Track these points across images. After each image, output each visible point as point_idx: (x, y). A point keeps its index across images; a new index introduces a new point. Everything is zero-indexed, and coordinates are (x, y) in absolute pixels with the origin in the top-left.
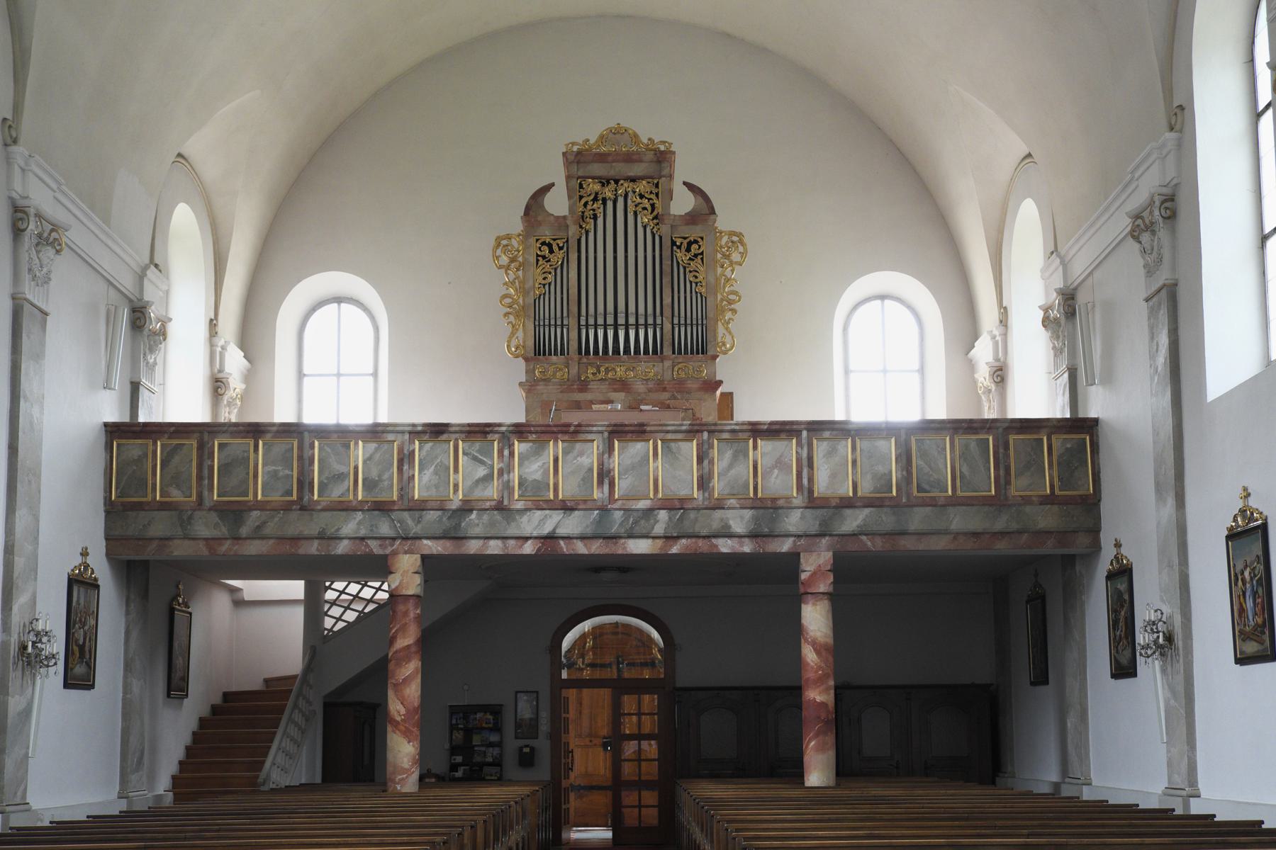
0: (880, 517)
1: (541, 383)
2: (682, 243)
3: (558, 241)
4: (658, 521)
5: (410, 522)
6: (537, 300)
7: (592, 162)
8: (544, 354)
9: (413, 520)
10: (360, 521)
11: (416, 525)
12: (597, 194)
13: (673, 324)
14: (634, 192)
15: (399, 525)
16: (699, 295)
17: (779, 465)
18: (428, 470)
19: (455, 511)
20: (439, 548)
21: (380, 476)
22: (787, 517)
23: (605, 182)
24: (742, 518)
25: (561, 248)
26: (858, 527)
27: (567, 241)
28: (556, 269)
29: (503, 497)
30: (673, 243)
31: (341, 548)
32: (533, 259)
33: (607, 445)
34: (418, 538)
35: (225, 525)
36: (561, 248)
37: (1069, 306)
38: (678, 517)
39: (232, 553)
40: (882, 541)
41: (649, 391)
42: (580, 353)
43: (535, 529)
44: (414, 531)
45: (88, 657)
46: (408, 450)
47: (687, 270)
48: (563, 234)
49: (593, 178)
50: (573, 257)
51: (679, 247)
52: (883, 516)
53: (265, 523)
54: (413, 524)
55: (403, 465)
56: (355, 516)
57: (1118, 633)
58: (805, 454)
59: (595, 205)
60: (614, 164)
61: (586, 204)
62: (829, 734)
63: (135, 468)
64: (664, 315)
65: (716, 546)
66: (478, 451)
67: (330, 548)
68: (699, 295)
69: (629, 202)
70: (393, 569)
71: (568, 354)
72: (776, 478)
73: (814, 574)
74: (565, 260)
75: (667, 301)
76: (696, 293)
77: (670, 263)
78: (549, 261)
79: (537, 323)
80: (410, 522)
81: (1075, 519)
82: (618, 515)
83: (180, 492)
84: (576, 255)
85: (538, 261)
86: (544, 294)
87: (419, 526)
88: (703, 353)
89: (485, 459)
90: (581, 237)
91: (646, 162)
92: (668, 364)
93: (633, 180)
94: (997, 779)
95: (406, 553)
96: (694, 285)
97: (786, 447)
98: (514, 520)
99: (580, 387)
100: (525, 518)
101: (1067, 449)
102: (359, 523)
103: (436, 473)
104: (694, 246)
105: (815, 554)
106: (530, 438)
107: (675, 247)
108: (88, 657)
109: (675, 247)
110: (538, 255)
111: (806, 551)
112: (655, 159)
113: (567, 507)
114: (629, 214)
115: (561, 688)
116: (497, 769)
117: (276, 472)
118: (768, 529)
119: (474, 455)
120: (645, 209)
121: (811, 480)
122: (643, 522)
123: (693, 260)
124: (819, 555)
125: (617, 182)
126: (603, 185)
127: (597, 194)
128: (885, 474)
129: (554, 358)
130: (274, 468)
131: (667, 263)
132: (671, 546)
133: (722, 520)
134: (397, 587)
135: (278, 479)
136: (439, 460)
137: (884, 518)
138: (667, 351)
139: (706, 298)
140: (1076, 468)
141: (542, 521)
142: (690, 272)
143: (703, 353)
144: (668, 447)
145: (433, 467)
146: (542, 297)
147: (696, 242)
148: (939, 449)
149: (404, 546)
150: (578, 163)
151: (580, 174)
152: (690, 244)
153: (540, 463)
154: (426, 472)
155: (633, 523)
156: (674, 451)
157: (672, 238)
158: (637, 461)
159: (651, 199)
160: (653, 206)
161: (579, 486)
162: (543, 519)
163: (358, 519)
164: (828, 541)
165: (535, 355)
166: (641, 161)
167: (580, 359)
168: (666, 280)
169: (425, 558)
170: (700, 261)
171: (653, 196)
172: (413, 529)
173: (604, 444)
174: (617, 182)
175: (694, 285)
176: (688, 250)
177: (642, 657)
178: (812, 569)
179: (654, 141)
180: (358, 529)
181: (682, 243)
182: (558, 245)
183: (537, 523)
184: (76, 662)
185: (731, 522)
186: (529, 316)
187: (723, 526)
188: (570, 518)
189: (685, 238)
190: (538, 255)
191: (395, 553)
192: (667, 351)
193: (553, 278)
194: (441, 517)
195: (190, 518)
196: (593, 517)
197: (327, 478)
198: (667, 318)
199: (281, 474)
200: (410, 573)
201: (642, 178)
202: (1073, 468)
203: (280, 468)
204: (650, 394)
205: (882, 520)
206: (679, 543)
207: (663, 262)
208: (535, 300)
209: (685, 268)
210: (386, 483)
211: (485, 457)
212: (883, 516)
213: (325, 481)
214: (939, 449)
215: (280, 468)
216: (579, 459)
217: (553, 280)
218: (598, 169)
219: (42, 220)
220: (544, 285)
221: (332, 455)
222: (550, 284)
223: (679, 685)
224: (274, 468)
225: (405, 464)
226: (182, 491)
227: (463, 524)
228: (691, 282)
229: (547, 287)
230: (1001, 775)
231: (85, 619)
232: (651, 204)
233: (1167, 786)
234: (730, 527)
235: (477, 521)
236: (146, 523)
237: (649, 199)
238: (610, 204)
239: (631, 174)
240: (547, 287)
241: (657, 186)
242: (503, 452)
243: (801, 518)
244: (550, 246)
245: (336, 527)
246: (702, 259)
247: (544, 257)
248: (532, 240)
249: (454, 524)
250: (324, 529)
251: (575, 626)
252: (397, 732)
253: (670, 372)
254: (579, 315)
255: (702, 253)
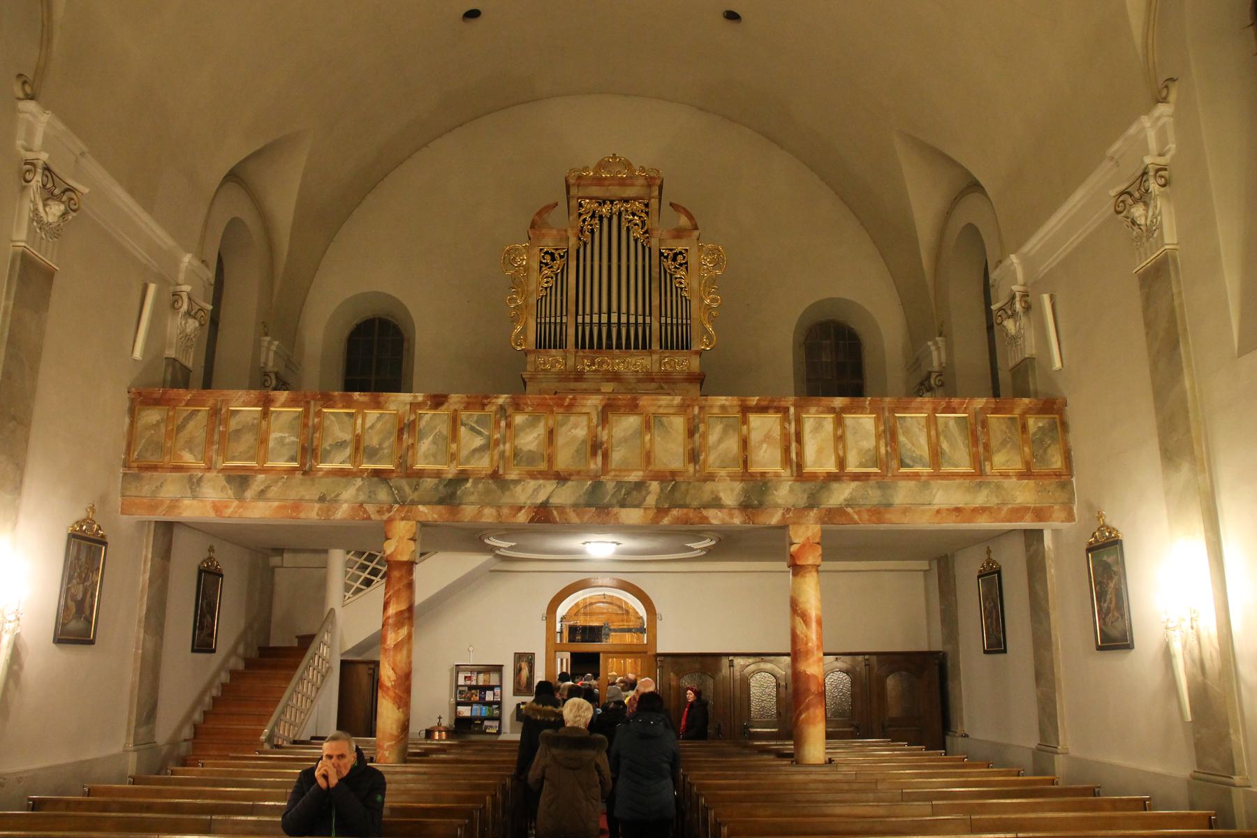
0: (866, 491)
1: (540, 373)
2: (668, 254)
3: (560, 251)
4: (650, 493)
5: (407, 489)
6: (539, 301)
7: (592, 185)
8: (545, 348)
9: (411, 487)
10: (359, 487)
11: (413, 492)
12: (594, 212)
13: (660, 324)
14: (627, 211)
15: (396, 492)
16: (684, 298)
17: (767, 440)
18: (427, 439)
19: (450, 480)
20: (435, 516)
21: (380, 444)
22: (776, 491)
23: (602, 202)
24: (732, 490)
25: (561, 257)
26: (845, 500)
27: (567, 251)
28: (557, 275)
29: (498, 467)
30: (661, 254)
31: (339, 514)
32: (536, 265)
33: (600, 418)
34: (413, 503)
35: (231, 489)
36: (561, 257)
37: (1026, 302)
38: (669, 489)
39: (237, 515)
40: (869, 515)
41: (639, 382)
42: (577, 346)
43: (528, 498)
44: (410, 498)
45: (88, 612)
46: (408, 420)
47: (673, 277)
48: (563, 245)
49: (591, 198)
50: (573, 264)
51: (666, 257)
52: (869, 490)
53: (269, 487)
54: (410, 492)
55: (403, 434)
56: (355, 482)
57: (1106, 605)
58: (793, 429)
59: (592, 222)
60: (610, 188)
61: (584, 220)
62: (819, 706)
63: (153, 432)
64: (653, 315)
65: (706, 518)
66: (477, 422)
67: (330, 513)
68: (684, 298)
69: (623, 219)
70: (390, 535)
71: (566, 347)
72: (765, 452)
73: (803, 546)
74: (566, 266)
75: (656, 302)
76: (681, 297)
77: (658, 270)
78: (552, 267)
79: (539, 320)
80: (407, 489)
81: (1050, 494)
82: (610, 486)
83: (192, 455)
84: (575, 262)
85: (541, 267)
86: (546, 295)
87: (416, 494)
88: (687, 348)
89: (482, 430)
90: (579, 248)
91: (637, 186)
92: (655, 357)
93: (626, 201)
94: (948, 740)
95: (403, 519)
96: (679, 290)
97: (774, 422)
98: (508, 489)
99: (576, 377)
100: (519, 488)
101: (1039, 428)
102: (359, 489)
103: (434, 442)
104: (680, 257)
105: (803, 527)
106: (526, 410)
107: (662, 258)
108: (88, 612)
109: (662, 258)
110: (541, 262)
111: (794, 523)
112: (646, 184)
113: (561, 478)
114: (622, 230)
115: (555, 651)
116: (496, 723)
117: (282, 438)
118: (758, 501)
119: (471, 426)
120: (636, 224)
121: (800, 454)
122: (635, 493)
123: (678, 268)
124: (808, 527)
125: (612, 202)
126: (600, 204)
127: (594, 212)
128: (870, 449)
129: (553, 351)
130: (281, 434)
131: (655, 270)
132: (663, 518)
133: (712, 492)
134: (392, 553)
135: (284, 445)
136: (438, 430)
137: (870, 492)
138: (655, 346)
139: (690, 301)
140: (1049, 445)
141: (536, 491)
142: (676, 278)
143: (687, 348)
144: (660, 421)
145: (431, 437)
146: (544, 298)
147: (681, 253)
148: (921, 427)
149: (401, 512)
150: (578, 186)
151: (580, 195)
152: (676, 255)
153: (535, 435)
154: (425, 441)
155: (625, 495)
156: (666, 425)
157: (660, 250)
158: (629, 434)
159: (642, 217)
160: (643, 223)
161: (573, 458)
162: (537, 489)
163: (357, 486)
164: (816, 514)
165: (536, 348)
166: (633, 185)
167: (576, 352)
168: (655, 285)
169: (424, 525)
170: (684, 269)
171: (643, 215)
172: (410, 495)
173: (598, 417)
174: (612, 202)
175: (679, 290)
176: (674, 259)
177: (625, 623)
178: (801, 542)
179: (645, 169)
180: (357, 494)
181: (668, 254)
182: (559, 254)
183: (530, 493)
184: (71, 617)
185: (722, 495)
186: (532, 314)
187: (713, 499)
188: (563, 488)
189: (671, 250)
190: (541, 262)
191: (390, 520)
192: (655, 346)
193: (554, 282)
194: (437, 486)
195: (200, 480)
196: (586, 487)
197: (330, 445)
198: (656, 318)
199: (287, 440)
200: (405, 540)
201: (635, 199)
202: (1046, 445)
203: (287, 435)
204: (639, 384)
205: (868, 494)
206: (669, 515)
207: (652, 269)
208: (538, 301)
209: (671, 275)
210: (386, 451)
211: (483, 428)
212: (869, 490)
213: (328, 448)
214: (921, 427)
215: (287, 435)
216: (573, 431)
217: (554, 284)
218: (596, 191)
219: (54, 176)
220: (546, 288)
221: (336, 424)
222: (551, 287)
223: (659, 651)
224: (281, 434)
225: (405, 433)
226: (194, 455)
227: (459, 492)
228: (676, 288)
229: (548, 289)
230: (950, 733)
231: (86, 574)
232: (642, 221)
233: (1196, 769)
234: (720, 499)
235: (472, 490)
236: (159, 484)
237: (640, 217)
238: (605, 221)
239: (625, 195)
240: (548, 289)
241: (647, 205)
242: (499, 424)
243: (790, 491)
244: (552, 255)
245: (336, 493)
246: (687, 268)
247: (546, 264)
248: (536, 250)
249: (449, 492)
250: (324, 495)
251: (568, 596)
252: (387, 697)
253: (658, 365)
254: (577, 314)
255: (686, 263)
